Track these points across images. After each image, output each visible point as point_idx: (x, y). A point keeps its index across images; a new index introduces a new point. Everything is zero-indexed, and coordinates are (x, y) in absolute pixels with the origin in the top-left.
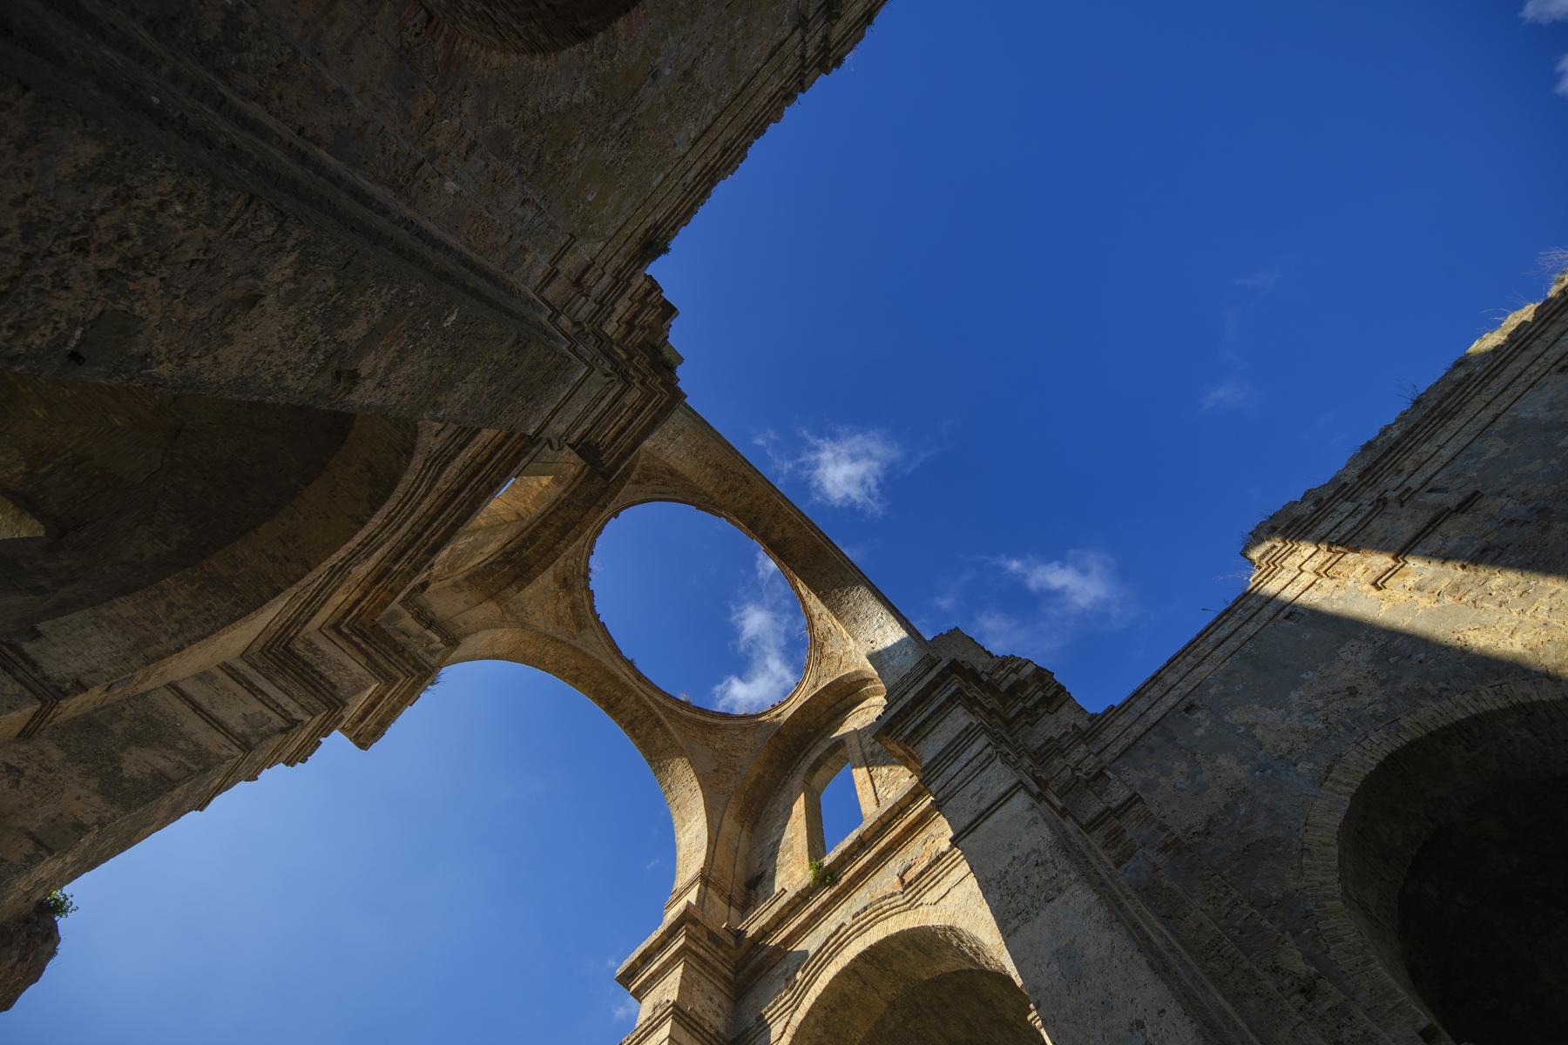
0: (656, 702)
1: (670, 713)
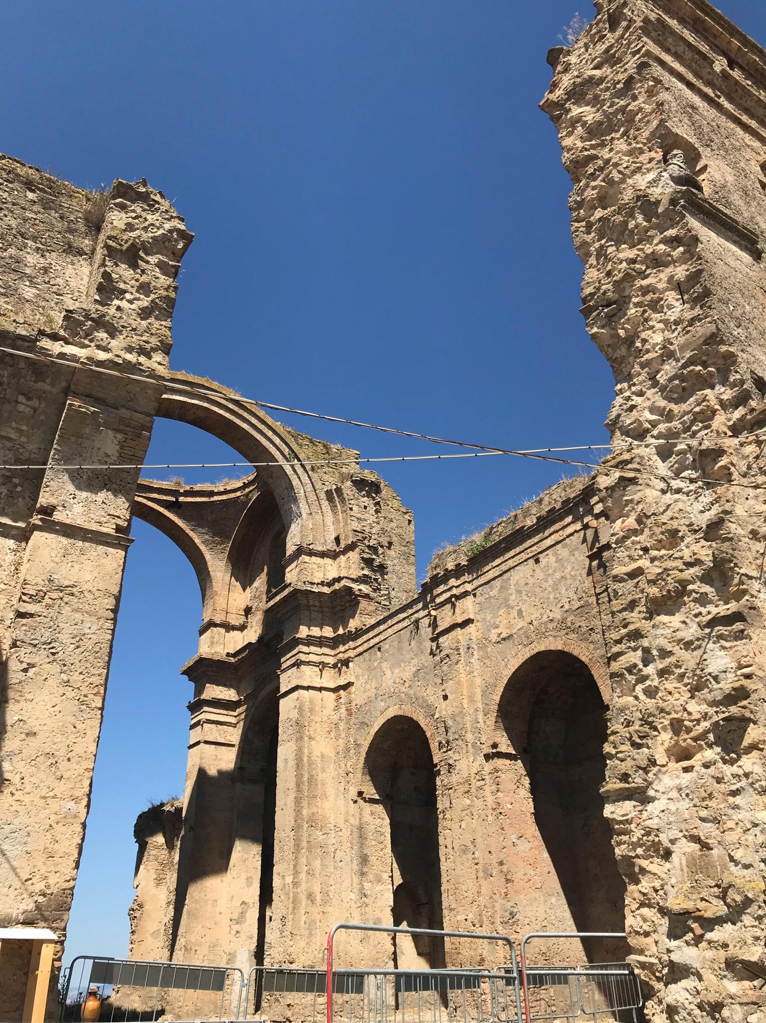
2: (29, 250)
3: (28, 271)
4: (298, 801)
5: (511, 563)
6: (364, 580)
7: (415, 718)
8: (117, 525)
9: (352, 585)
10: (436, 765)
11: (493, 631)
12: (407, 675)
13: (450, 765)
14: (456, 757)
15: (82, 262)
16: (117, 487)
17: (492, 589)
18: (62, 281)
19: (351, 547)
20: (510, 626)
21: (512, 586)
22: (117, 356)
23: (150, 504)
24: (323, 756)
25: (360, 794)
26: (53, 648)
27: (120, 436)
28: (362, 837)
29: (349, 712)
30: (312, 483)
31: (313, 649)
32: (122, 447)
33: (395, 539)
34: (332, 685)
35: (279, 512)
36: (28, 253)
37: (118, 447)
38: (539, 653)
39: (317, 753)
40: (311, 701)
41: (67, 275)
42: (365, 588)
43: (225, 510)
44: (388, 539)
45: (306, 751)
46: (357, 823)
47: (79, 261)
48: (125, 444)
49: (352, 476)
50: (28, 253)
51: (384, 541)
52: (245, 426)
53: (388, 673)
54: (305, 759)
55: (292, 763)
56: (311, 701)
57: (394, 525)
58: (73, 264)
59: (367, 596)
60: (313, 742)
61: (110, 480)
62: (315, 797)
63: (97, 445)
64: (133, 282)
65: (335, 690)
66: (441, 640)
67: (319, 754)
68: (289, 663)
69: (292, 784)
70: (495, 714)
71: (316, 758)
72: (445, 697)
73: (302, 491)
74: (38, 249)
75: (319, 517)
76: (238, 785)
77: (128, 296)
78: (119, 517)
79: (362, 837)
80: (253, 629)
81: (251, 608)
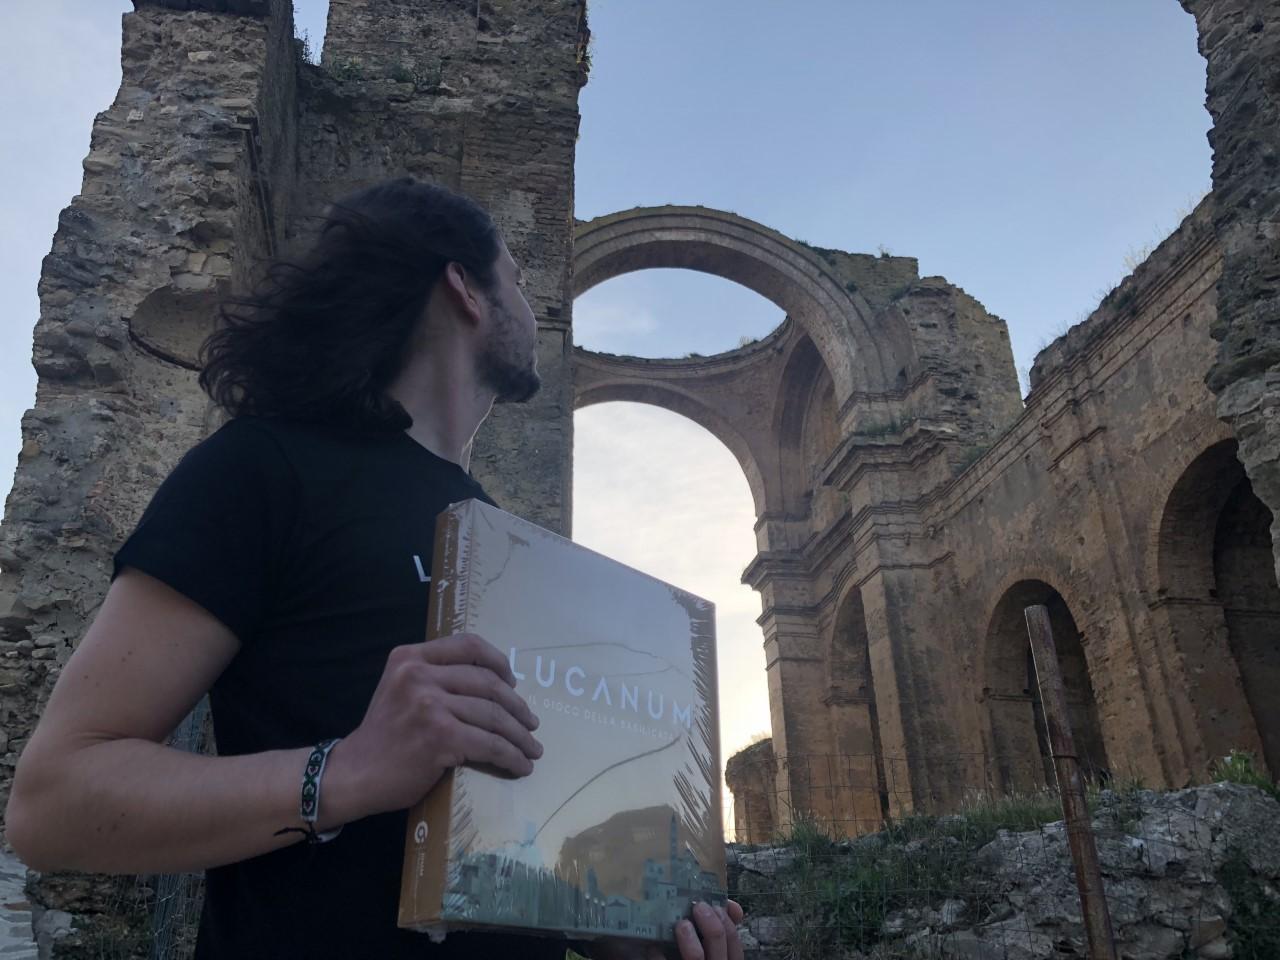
0: (671, 381)
1: (687, 382)
2: (403, 16)
3: (404, 40)
4: (904, 709)
5: (1147, 334)
6: (950, 416)
7: (1044, 580)
8: (548, 308)
9: (930, 428)
10: (1082, 634)
11: (1137, 436)
12: (1025, 526)
13: (1101, 628)
14: (1109, 617)
15: (466, 15)
16: (540, 262)
17: (1125, 377)
18: (445, 42)
19: (922, 380)
20: (1161, 422)
21: (1156, 365)
22: (508, 95)
23: (668, 386)
24: (929, 651)
25: (986, 690)
26: (491, 456)
27: (532, 196)
28: (1000, 748)
29: (957, 591)
30: (857, 309)
31: (893, 518)
32: (537, 212)
33: (983, 361)
34: (926, 561)
35: (821, 358)
36: (403, 19)
37: (532, 212)
38: (1210, 448)
39: (920, 647)
40: (901, 585)
41: (451, 33)
42: (948, 429)
43: (757, 376)
44: (975, 362)
45: (905, 646)
46: (987, 727)
47: (462, 15)
48: (541, 206)
49: (909, 289)
50: (403, 19)
51: (970, 364)
52: (758, 254)
53: (999, 531)
54: (906, 656)
55: (889, 664)
56: (901, 585)
57: (979, 342)
58: (455, 20)
59: (950, 438)
60: (913, 635)
61: (530, 254)
62: (927, 702)
63: (507, 214)
64: (521, 10)
65: (930, 566)
66: (1062, 465)
67: (923, 649)
68: (864, 541)
69: (893, 689)
70: (1156, 549)
71: (919, 654)
72: (1081, 540)
73: (844, 323)
74: (413, 11)
75: (873, 352)
76: (834, 708)
77: (515, 28)
78: (549, 299)
79: (1000, 748)
80: (819, 518)
81: (812, 491)
